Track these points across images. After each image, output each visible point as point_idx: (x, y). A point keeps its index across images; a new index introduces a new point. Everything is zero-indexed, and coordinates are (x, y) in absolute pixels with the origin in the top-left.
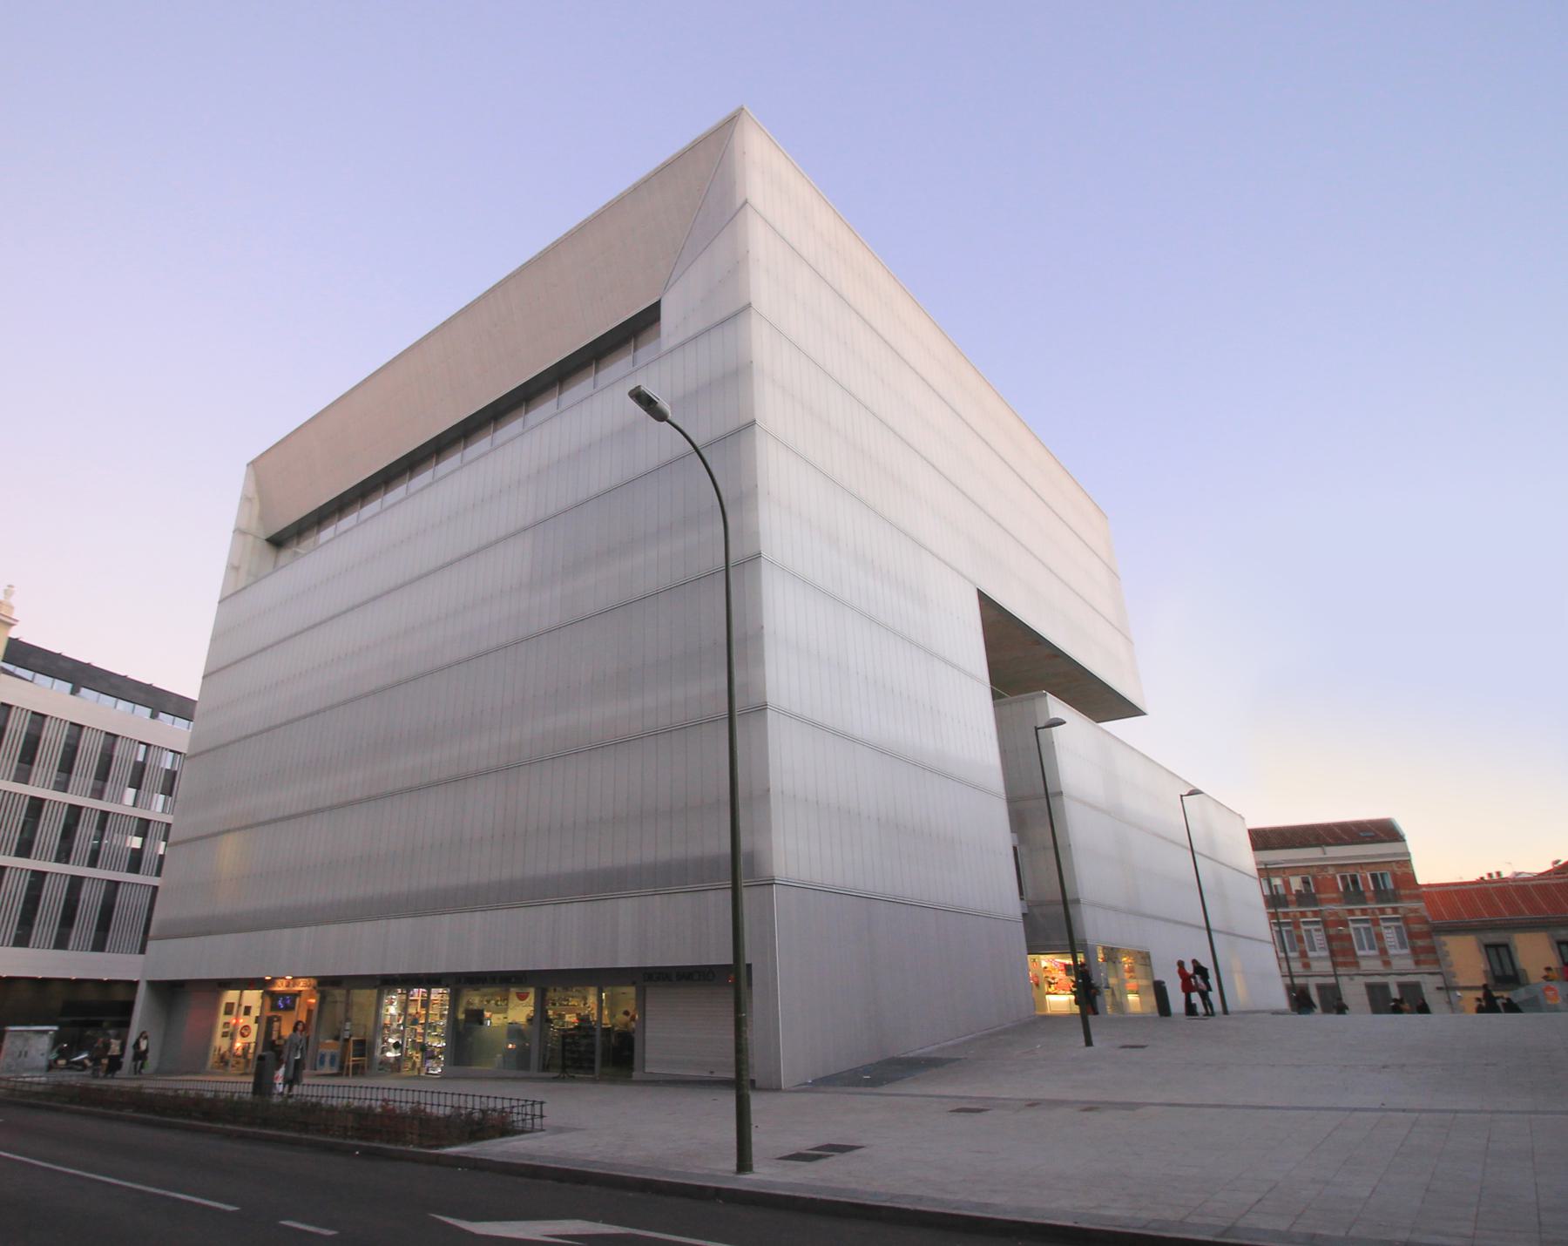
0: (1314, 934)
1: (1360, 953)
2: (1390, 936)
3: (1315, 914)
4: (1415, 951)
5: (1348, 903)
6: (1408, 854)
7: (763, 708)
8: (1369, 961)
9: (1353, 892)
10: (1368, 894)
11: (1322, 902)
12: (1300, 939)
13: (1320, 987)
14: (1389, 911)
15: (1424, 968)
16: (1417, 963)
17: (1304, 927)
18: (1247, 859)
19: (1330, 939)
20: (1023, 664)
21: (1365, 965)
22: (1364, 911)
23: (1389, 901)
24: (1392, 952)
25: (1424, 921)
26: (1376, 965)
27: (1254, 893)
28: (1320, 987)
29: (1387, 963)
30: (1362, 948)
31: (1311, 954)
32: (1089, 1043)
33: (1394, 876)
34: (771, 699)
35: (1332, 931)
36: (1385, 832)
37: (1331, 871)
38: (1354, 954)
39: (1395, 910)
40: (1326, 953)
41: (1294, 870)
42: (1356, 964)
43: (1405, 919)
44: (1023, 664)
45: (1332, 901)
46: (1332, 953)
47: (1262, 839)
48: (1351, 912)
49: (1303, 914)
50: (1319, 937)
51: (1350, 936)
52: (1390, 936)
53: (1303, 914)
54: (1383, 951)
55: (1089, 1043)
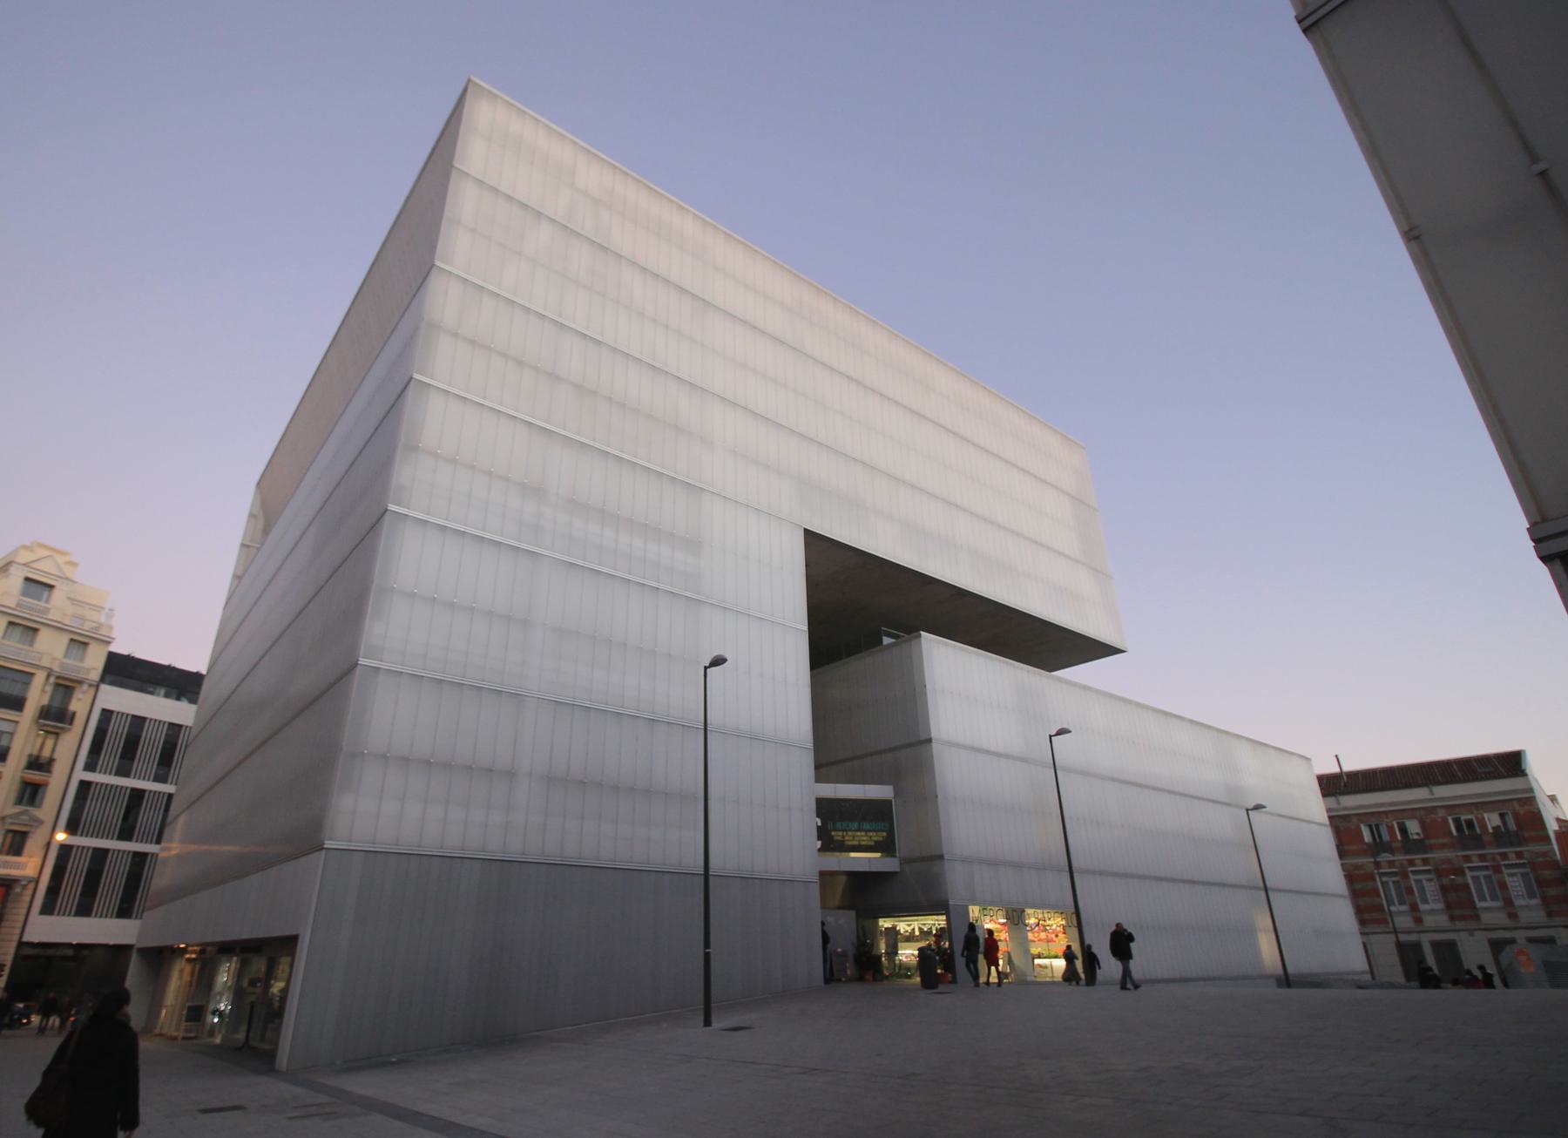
2: (1515, 884)
3: (1425, 862)
5: (1465, 848)
6: (1531, 790)
7: (930, 740)
9: (1469, 836)
10: (1486, 838)
11: (1430, 848)
12: (1410, 891)
13: (1436, 945)
14: (1512, 856)
15: (1460, 925)
18: (1316, 808)
19: (1444, 889)
20: (864, 611)
21: (1486, 918)
22: (1482, 858)
23: (1512, 845)
24: (1518, 902)
25: (1554, 864)
26: (1501, 918)
27: (1325, 842)
28: (1436, 945)
29: (1513, 916)
30: (1482, 898)
31: (1423, 907)
32: (707, 1023)
33: (1516, 816)
34: (934, 734)
35: (1445, 881)
36: (1512, 764)
38: (1380, 908)
39: (1519, 855)
40: (1440, 906)
41: (1412, 813)
42: (1477, 918)
43: (1532, 865)
44: (864, 611)
45: (1442, 847)
46: (1448, 906)
47: (1332, 785)
48: (1467, 859)
50: (1431, 888)
51: (1467, 886)
52: (1515, 884)
53: (1412, 863)
54: (1508, 902)
55: (707, 1023)
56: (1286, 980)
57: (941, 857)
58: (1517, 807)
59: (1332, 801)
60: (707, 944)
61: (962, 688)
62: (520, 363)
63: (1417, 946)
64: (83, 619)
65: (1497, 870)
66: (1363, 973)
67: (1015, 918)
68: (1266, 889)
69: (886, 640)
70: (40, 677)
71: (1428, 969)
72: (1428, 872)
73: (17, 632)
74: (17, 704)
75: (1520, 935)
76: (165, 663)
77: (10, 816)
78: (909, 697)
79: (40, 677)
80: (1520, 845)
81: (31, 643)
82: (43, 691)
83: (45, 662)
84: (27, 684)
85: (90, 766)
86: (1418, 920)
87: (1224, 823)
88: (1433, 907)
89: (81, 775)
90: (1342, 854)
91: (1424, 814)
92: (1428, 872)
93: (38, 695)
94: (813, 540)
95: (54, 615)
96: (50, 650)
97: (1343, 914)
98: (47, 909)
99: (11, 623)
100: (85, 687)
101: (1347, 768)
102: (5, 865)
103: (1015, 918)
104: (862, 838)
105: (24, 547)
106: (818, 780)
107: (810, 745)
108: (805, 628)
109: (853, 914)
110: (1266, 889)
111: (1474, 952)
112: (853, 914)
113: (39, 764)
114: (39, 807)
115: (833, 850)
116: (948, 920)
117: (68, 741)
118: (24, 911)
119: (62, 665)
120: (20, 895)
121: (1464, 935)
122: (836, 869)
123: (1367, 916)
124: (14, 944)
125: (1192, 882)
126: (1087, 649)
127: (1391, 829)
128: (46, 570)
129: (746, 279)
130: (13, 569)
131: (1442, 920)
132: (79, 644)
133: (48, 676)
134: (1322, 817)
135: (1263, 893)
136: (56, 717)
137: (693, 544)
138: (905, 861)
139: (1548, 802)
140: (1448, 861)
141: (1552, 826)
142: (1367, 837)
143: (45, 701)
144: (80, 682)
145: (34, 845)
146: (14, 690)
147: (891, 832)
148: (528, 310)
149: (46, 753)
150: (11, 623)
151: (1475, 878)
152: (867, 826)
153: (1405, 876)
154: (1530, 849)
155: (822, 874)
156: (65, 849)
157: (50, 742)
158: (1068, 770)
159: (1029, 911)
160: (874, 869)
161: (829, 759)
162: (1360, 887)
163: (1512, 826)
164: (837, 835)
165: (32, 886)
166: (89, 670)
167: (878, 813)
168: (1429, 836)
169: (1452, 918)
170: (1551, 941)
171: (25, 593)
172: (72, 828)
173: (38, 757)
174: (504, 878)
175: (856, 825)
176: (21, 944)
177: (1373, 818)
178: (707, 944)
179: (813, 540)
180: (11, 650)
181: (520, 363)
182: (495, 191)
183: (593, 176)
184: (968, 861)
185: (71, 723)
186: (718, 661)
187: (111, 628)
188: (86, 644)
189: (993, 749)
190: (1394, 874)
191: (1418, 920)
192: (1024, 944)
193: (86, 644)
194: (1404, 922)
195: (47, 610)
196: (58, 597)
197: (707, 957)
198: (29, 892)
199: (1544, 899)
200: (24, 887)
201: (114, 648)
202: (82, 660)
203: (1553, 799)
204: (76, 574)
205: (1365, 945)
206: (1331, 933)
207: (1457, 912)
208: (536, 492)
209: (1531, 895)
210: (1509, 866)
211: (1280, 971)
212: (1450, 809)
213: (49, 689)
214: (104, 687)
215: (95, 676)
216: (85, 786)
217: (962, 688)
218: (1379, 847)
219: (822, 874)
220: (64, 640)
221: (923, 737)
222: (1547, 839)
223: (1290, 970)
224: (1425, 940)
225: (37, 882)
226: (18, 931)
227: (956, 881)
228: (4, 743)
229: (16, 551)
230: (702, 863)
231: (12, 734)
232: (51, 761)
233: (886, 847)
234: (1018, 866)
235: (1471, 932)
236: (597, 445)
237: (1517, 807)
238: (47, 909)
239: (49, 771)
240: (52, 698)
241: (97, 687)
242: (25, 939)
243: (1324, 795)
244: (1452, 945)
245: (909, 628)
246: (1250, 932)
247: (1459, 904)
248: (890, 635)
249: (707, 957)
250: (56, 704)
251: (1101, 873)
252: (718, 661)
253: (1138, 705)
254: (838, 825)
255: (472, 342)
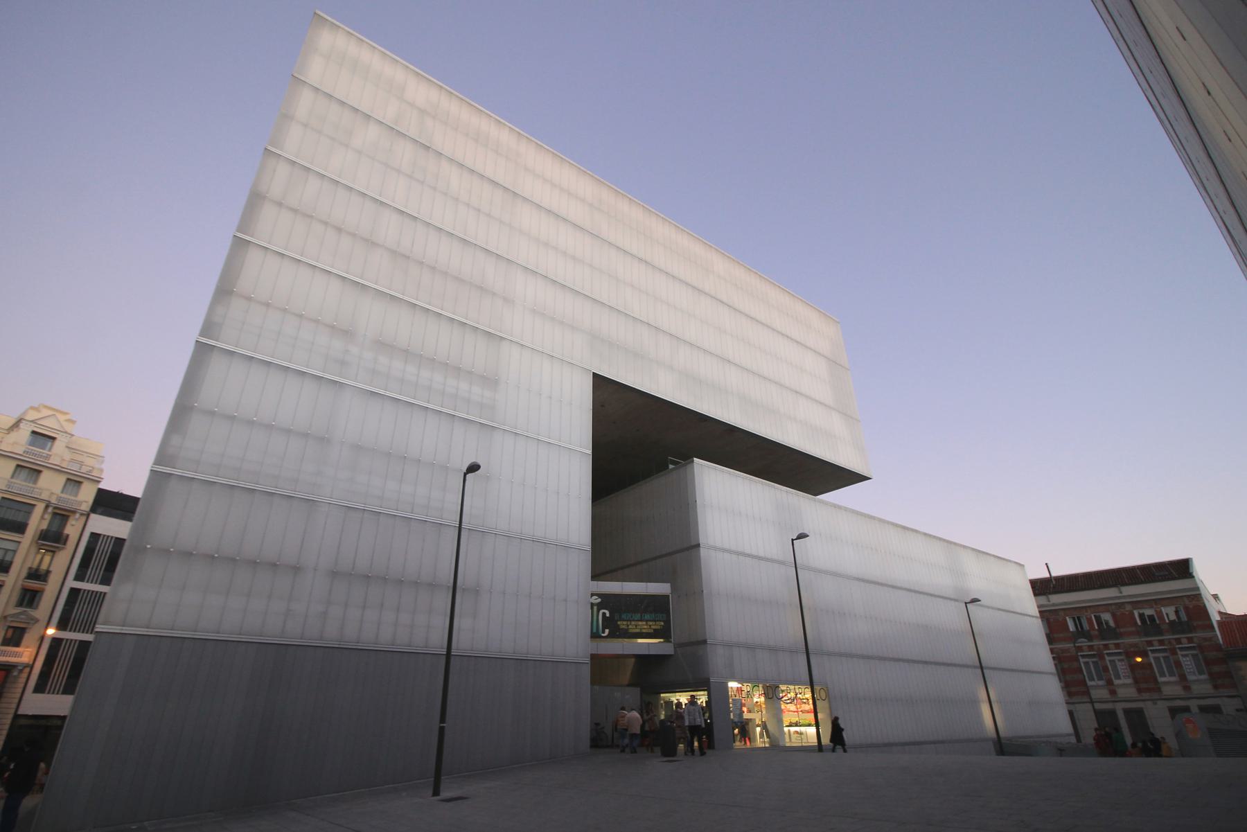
0: (1119, 664)
1: (1161, 679)
2: (1188, 663)
4: (1213, 677)
5: (1146, 635)
6: (1198, 589)
7: (698, 545)
8: (1169, 684)
9: (1151, 626)
10: (1164, 627)
11: (1121, 635)
12: (1106, 669)
13: (1127, 712)
14: (1184, 641)
15: (1146, 696)
16: (1216, 687)
17: (1107, 658)
18: (1029, 604)
20: (642, 445)
21: (1167, 691)
22: (1161, 642)
23: (1183, 632)
24: (1191, 678)
25: (1218, 647)
26: (1178, 690)
27: (1036, 630)
28: (1127, 712)
29: (1187, 688)
30: (1163, 675)
31: (1116, 682)
33: (1186, 609)
34: (702, 541)
36: (1182, 568)
37: (1128, 607)
38: (1084, 683)
39: (1190, 640)
40: (1129, 681)
41: (1106, 608)
42: (1159, 690)
43: (1200, 648)
45: (1130, 634)
46: (1136, 681)
47: (1041, 587)
48: (1150, 643)
49: (1106, 647)
50: (1122, 667)
51: (1150, 665)
52: (1188, 663)
53: (1106, 647)
54: (1183, 677)
55: (436, 792)
56: (1002, 746)
57: (705, 642)
58: (1187, 602)
59: (1043, 600)
60: (443, 720)
61: (727, 505)
62: (339, 230)
63: (1113, 713)
64: (81, 464)
65: (1173, 652)
66: (1069, 735)
67: (772, 693)
68: (982, 668)
69: (671, 466)
70: (40, 507)
71: (1108, 742)
72: (1119, 654)
73: (24, 474)
74: (20, 528)
75: (1194, 704)
76: (116, 490)
77: (13, 615)
78: (683, 511)
79: (40, 507)
80: (1191, 632)
81: (35, 482)
82: (42, 518)
83: (44, 496)
84: (29, 513)
85: (80, 577)
86: (1113, 692)
87: (952, 616)
88: (1125, 685)
89: (71, 583)
90: (1051, 639)
91: (1115, 608)
92: (1119, 654)
93: (37, 522)
94: (600, 382)
95: (55, 460)
96: (50, 486)
97: (1052, 688)
98: (40, 688)
99: (18, 466)
100: (77, 515)
101: (1054, 574)
102: (4, 654)
103: (772, 693)
104: (643, 626)
105: (32, 408)
106: (595, 576)
107: (589, 548)
108: (590, 452)
109: (638, 690)
110: (982, 668)
111: (1159, 720)
112: (638, 690)
113: (38, 575)
114: (36, 608)
115: (619, 637)
116: (709, 695)
117: (62, 558)
118: (20, 690)
119: (59, 499)
120: (17, 677)
121: (1149, 703)
122: (620, 652)
123: (1073, 689)
124: (11, 716)
125: (926, 663)
126: (841, 477)
127: (1090, 621)
128: (49, 425)
129: (395, 72)
130: (22, 425)
131: (1131, 692)
132: (74, 482)
133: (47, 507)
134: (1035, 611)
135: (979, 671)
136: (53, 538)
137: (490, 381)
138: (678, 646)
139: (1212, 599)
140: (1135, 645)
141: (1215, 617)
142: (1072, 628)
143: (44, 526)
144: (74, 512)
145: (30, 639)
146: (19, 518)
147: (667, 622)
148: (351, 189)
149: (44, 567)
150: (18, 466)
151: (1157, 659)
152: (647, 616)
153: (1101, 657)
154: (1199, 634)
155: (594, 657)
156: (56, 642)
157: (47, 559)
158: (809, 569)
159: (783, 687)
160: (652, 652)
161: (604, 563)
162: (1066, 668)
163: (1184, 617)
164: (622, 625)
165: (27, 670)
166: (80, 503)
167: (657, 605)
168: (1121, 624)
169: (1140, 691)
170: (1216, 709)
171: (32, 443)
172: (62, 625)
173: (37, 570)
174: (277, 662)
175: (638, 616)
176: (17, 717)
177: (1077, 612)
178: (443, 720)
179: (600, 382)
180: (22, 485)
181: (339, 230)
182: (330, 96)
183: (422, 92)
184: (729, 645)
185: (65, 543)
186: (474, 468)
187: (102, 470)
188: (80, 483)
189: (754, 552)
190: (1093, 656)
191: (1113, 692)
192: (778, 715)
193: (80, 483)
194: (1100, 693)
195: (48, 457)
196: (59, 447)
197: (442, 730)
198: (25, 675)
199: (1211, 674)
200: (21, 671)
201: (103, 486)
202: (76, 495)
203: (1216, 597)
204: (69, 427)
205: (1071, 713)
206: (1043, 704)
207: (1144, 686)
208: (347, 334)
209: (1201, 673)
210: (1181, 649)
211: (994, 735)
212: (1136, 604)
213: (48, 517)
214: (93, 516)
215: (86, 507)
216: (74, 592)
217: (727, 505)
218: (1081, 633)
219: (594, 657)
220: (63, 479)
221: (693, 543)
222: (1212, 627)
223: (1002, 734)
224: (1119, 708)
225: (32, 667)
226: (14, 706)
227: (717, 660)
228: (8, 558)
229: (25, 413)
230: (445, 645)
231: (15, 551)
232: (48, 572)
233: (664, 633)
234: (773, 650)
235: (1154, 701)
236: (406, 298)
237: (1187, 602)
238: (40, 688)
239: (45, 581)
240: (50, 524)
241: (88, 516)
242: (20, 712)
243: (1035, 595)
244: (1140, 712)
245: (687, 457)
246: (975, 703)
247: (1145, 680)
248: (673, 463)
249: (442, 730)
250: (54, 529)
251: (841, 655)
252: (474, 468)
253: (881, 521)
254: (624, 616)
255: (295, 211)
